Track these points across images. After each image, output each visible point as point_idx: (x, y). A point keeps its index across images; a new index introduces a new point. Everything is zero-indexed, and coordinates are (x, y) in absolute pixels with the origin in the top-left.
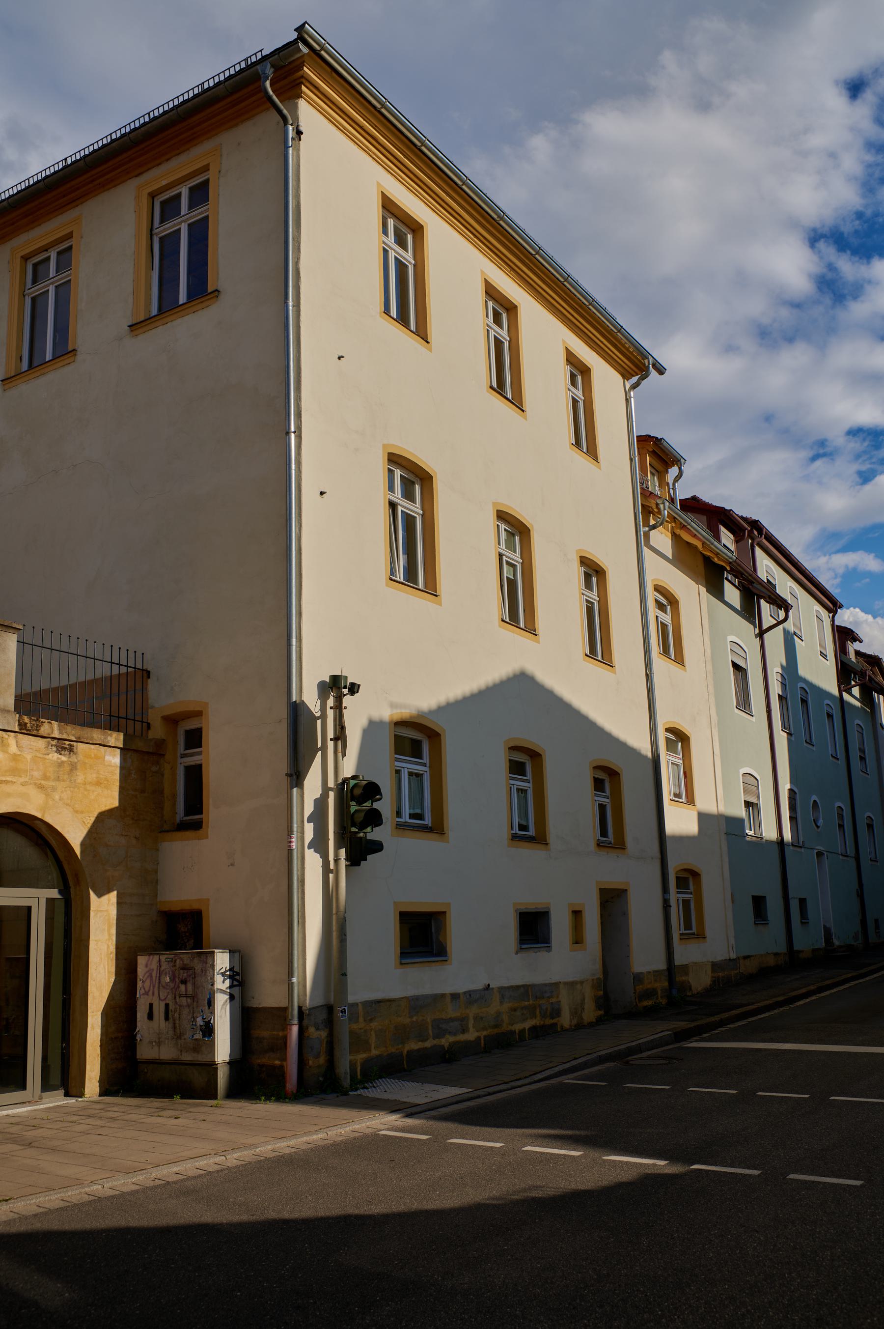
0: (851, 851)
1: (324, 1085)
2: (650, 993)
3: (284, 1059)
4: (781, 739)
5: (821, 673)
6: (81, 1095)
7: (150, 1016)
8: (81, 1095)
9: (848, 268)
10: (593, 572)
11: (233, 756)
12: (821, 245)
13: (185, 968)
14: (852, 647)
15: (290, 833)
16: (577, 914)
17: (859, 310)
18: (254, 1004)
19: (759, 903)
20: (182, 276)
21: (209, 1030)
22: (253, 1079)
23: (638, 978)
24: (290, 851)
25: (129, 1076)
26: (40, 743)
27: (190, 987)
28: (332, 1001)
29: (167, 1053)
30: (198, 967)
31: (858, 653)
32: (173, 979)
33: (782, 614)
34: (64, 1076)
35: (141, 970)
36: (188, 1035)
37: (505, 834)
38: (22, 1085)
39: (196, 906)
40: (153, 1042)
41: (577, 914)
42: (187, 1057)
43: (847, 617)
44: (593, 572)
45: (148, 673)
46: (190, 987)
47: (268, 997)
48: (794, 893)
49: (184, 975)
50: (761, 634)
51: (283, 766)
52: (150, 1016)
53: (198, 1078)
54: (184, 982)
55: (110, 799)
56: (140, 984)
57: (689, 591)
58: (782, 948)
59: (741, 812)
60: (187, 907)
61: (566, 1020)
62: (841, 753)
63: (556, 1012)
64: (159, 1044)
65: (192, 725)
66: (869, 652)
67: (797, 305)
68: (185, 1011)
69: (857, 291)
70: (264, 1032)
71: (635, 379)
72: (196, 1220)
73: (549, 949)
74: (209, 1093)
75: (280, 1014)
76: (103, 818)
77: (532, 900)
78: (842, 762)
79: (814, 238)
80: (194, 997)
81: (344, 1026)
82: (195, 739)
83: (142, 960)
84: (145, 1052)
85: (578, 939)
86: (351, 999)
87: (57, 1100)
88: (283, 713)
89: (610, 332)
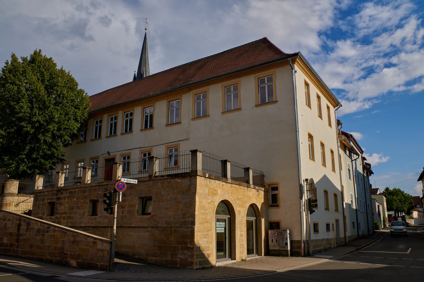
0: (366, 212)
1: (308, 254)
2: (342, 242)
3: (301, 249)
4: (355, 185)
5: (360, 169)
6: (235, 259)
7: (272, 241)
8: (235, 259)
9: (330, 43)
10: (332, 152)
11: (283, 193)
12: (322, 37)
13: (280, 233)
14: (365, 161)
15: (301, 208)
16: (333, 225)
17: (333, 55)
18: (293, 240)
19: (353, 223)
20: (266, 98)
21: (287, 244)
22: (295, 253)
23: (341, 238)
24: (301, 211)
25: (268, 253)
26: (255, 190)
27: (282, 236)
28: (308, 239)
29: (277, 248)
30: (284, 233)
31: (366, 163)
32: (278, 234)
33: (357, 157)
34: (259, 253)
35: (269, 233)
36: (282, 245)
37: (324, 208)
38: (253, 254)
39: (278, 221)
40: (273, 246)
41: (333, 225)
42: (281, 249)
43: (364, 155)
44: (332, 152)
45: (264, 176)
46: (282, 236)
47: (296, 238)
48: (359, 222)
49: (280, 234)
50: (352, 161)
51: (298, 195)
52: (272, 241)
53: (284, 253)
54: (280, 235)
55: (263, 201)
56: (269, 236)
57: (342, 152)
58: (356, 234)
59: (350, 203)
60: (276, 221)
61: (333, 246)
62: (364, 188)
63: (331, 245)
64: (275, 246)
65: (276, 186)
66: (367, 162)
67: (316, 54)
68: (281, 241)
69: (332, 50)
70: (295, 245)
71: (336, 108)
72: (335, 269)
73: (330, 231)
74: (287, 255)
75: (299, 242)
76: (262, 204)
77: (328, 222)
78: (364, 190)
79: (320, 34)
80: (283, 238)
81: (311, 245)
82: (276, 189)
83: (270, 232)
84: (271, 248)
85: (333, 230)
86: (312, 239)
87: (257, 257)
88: (298, 185)
89: (334, 99)
